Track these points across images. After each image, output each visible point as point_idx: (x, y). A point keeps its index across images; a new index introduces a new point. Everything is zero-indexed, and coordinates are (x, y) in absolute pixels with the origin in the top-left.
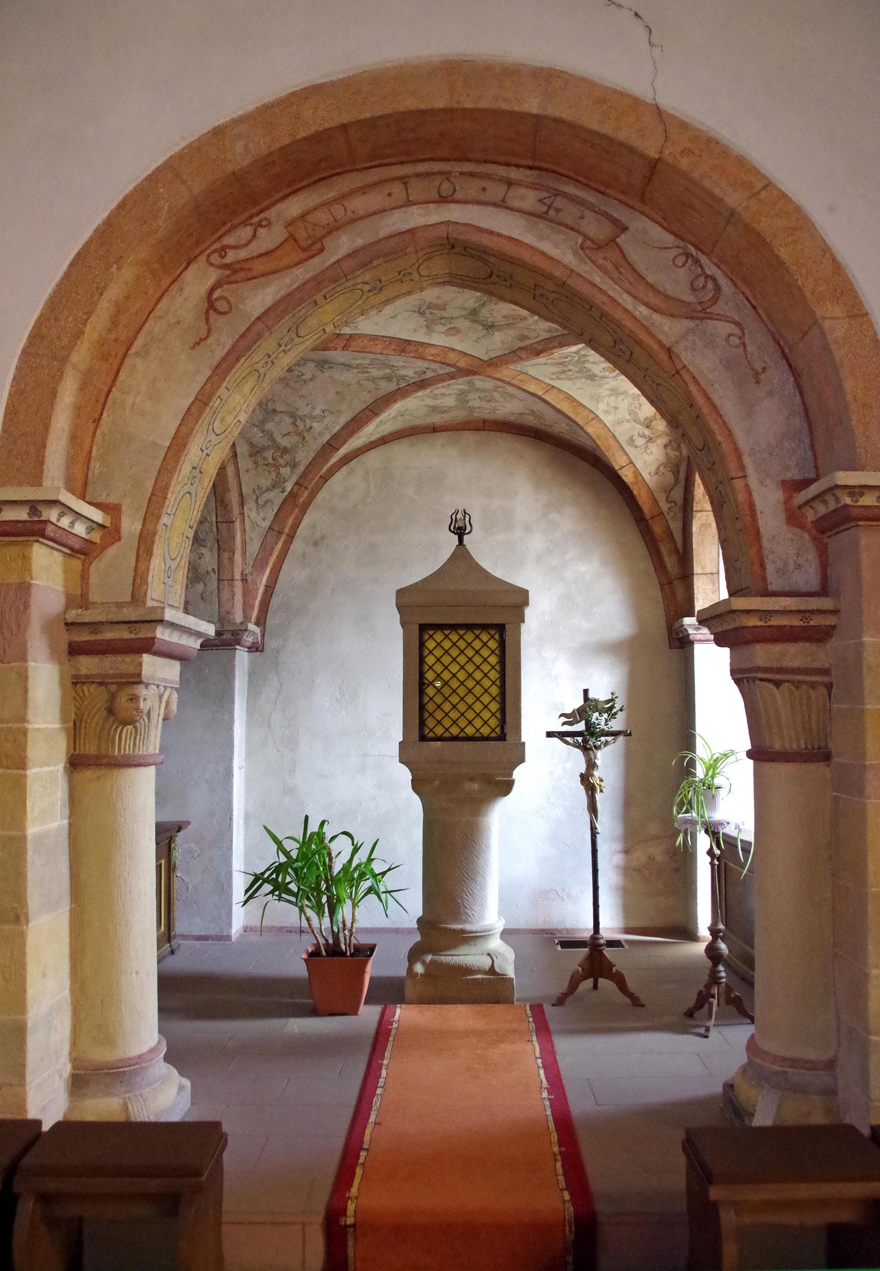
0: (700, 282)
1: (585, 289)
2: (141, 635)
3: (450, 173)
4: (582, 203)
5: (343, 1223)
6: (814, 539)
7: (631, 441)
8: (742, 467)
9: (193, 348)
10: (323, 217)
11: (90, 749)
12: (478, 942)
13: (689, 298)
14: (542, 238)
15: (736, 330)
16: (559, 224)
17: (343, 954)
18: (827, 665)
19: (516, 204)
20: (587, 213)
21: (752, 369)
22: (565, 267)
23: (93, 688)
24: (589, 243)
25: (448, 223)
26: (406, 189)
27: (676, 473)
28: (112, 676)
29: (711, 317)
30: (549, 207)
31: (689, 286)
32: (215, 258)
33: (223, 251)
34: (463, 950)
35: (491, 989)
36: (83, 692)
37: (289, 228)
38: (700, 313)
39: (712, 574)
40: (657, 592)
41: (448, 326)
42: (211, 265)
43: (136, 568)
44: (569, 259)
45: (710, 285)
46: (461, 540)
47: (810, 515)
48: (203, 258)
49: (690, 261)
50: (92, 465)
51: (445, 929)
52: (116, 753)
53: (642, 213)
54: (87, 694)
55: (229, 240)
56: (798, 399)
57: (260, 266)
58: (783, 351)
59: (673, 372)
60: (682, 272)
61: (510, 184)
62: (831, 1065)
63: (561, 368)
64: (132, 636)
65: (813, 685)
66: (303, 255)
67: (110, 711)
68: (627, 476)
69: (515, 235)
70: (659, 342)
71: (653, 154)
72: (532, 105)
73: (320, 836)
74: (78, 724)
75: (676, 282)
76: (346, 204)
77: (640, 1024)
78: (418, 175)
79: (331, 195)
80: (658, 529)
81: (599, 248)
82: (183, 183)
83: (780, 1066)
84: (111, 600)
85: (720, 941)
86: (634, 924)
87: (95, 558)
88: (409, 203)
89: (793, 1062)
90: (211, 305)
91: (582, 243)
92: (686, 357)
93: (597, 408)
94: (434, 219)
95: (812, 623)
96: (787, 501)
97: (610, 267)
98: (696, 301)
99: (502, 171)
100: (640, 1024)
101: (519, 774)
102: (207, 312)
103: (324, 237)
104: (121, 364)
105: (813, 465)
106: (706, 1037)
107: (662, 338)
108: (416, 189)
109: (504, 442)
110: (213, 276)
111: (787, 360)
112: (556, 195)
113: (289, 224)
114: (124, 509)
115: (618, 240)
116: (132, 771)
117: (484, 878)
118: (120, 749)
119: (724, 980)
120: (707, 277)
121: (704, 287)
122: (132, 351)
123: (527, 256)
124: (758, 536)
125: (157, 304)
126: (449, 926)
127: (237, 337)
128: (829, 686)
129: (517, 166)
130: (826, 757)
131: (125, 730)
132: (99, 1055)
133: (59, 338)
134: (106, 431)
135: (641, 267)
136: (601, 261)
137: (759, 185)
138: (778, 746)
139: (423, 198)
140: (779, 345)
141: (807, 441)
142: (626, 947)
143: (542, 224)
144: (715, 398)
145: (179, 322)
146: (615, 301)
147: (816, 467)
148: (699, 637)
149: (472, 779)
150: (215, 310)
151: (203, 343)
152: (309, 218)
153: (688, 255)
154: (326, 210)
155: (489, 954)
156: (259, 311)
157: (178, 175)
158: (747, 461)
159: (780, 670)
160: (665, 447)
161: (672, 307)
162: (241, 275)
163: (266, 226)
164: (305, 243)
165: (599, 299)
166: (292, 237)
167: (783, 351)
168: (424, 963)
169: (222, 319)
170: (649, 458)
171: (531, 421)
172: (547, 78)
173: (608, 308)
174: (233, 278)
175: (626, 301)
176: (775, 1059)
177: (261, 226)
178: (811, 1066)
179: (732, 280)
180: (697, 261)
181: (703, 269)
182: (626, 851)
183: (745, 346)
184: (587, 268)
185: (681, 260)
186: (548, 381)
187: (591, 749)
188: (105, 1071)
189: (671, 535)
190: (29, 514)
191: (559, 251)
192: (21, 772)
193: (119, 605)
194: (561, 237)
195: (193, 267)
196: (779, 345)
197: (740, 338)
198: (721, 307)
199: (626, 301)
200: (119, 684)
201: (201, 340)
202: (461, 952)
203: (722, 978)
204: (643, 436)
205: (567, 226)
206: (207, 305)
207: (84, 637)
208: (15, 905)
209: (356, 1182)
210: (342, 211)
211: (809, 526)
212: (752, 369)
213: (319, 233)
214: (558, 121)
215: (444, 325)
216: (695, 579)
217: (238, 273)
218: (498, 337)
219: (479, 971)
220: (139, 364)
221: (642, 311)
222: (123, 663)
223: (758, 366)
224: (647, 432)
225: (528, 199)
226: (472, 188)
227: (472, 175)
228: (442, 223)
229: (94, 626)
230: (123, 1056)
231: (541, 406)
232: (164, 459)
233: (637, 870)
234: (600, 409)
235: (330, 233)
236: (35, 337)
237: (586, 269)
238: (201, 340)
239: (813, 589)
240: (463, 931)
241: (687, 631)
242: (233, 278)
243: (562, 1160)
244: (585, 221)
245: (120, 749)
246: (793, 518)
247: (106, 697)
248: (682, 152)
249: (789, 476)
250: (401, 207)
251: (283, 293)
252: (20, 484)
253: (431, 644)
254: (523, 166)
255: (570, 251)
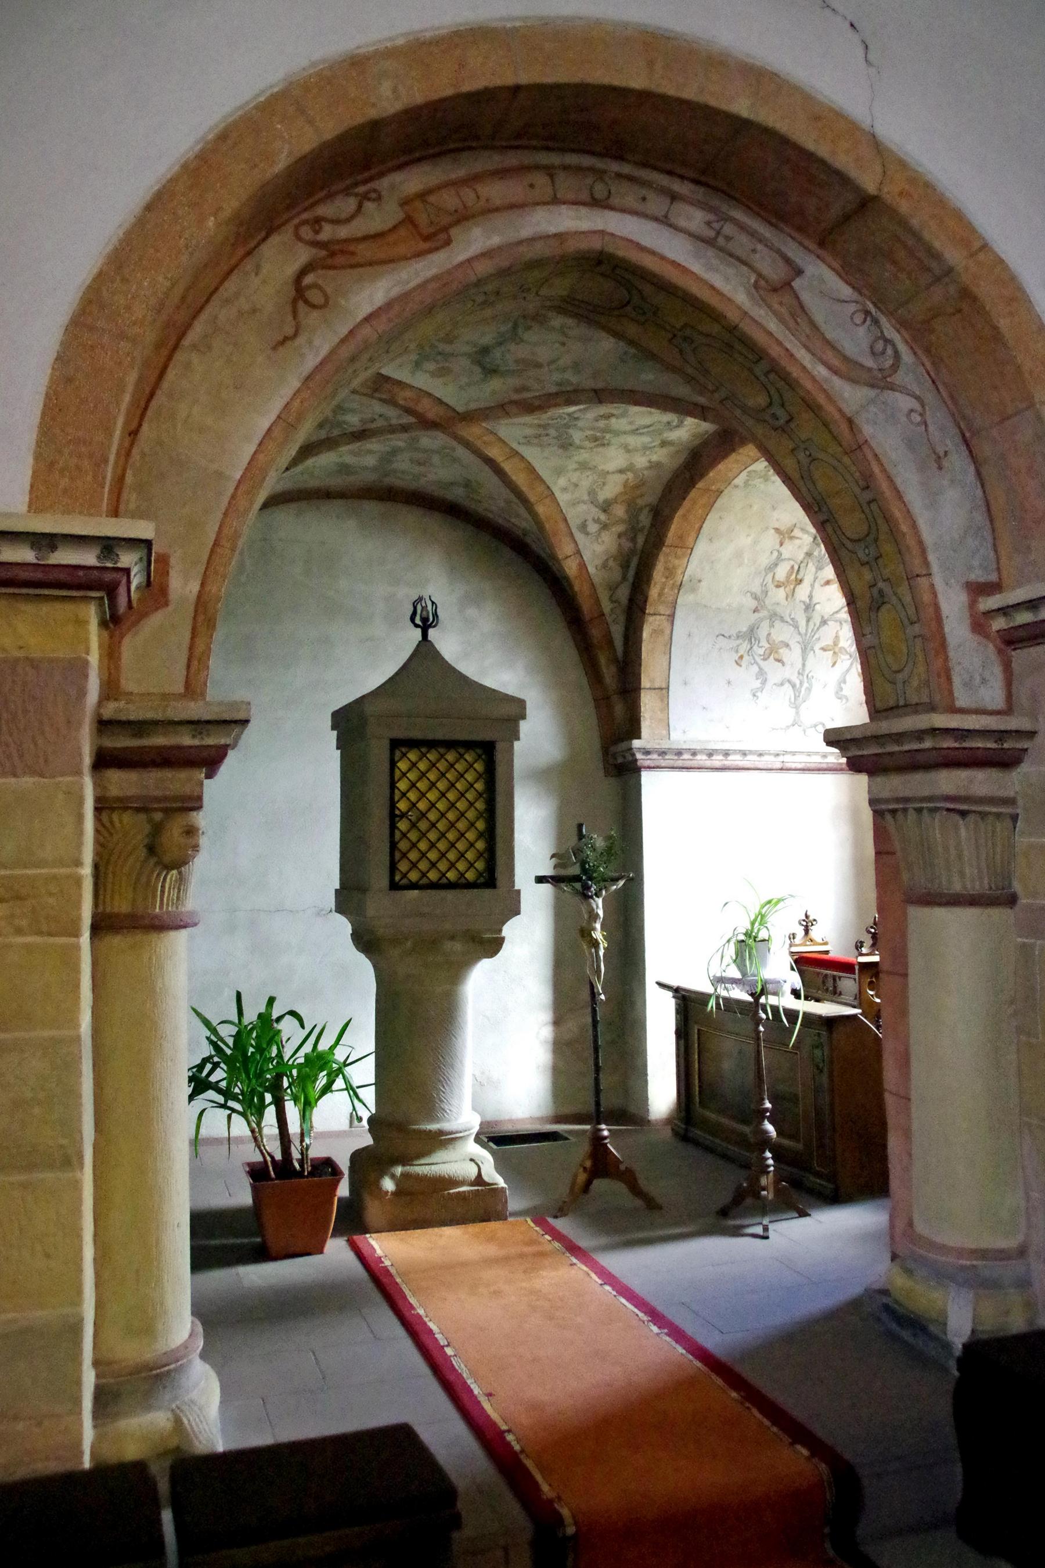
0: (879, 346)
1: (760, 338)
2: (210, 741)
3: (605, 172)
4: (753, 234)
5: (561, 1535)
6: (1000, 652)
7: (583, 527)
8: (926, 564)
9: (274, 348)
10: (449, 200)
11: (121, 905)
12: (458, 1144)
13: (869, 362)
14: (710, 268)
15: (916, 405)
16: (731, 255)
17: (300, 1174)
18: (1012, 794)
19: (682, 223)
20: (760, 247)
21: (935, 453)
22: (739, 308)
23: (127, 818)
24: (762, 283)
25: (602, 233)
26: (553, 182)
27: (625, 566)
28: (157, 799)
29: (892, 388)
30: (718, 233)
31: (868, 350)
32: (306, 232)
33: (317, 223)
34: (440, 1156)
35: (478, 1206)
36: (112, 822)
37: (406, 207)
38: (881, 381)
39: (662, 689)
40: (590, 710)
41: (441, 365)
42: (299, 238)
43: (191, 648)
44: (741, 298)
45: (889, 351)
46: (425, 635)
47: (999, 624)
48: (289, 228)
49: (868, 322)
50: (125, 496)
51: (414, 1130)
52: (157, 910)
53: (818, 257)
54: (118, 825)
55: (324, 210)
56: (979, 492)
57: (364, 251)
58: (963, 436)
59: (855, 447)
60: (861, 331)
61: (674, 197)
62: (1022, 1252)
63: (541, 431)
64: (196, 742)
65: (998, 815)
66: (424, 246)
67: (151, 850)
68: (571, 568)
69: (681, 259)
70: (840, 410)
71: (871, 188)
72: (742, 107)
73: (266, 1021)
74: (102, 869)
75: (855, 341)
76: (479, 188)
77: (677, 1231)
78: (566, 168)
79: (461, 173)
80: (595, 633)
81: (775, 290)
82: (311, 122)
83: (967, 1260)
84: (155, 691)
85: (766, 1122)
86: (567, 1110)
87: (129, 630)
88: (555, 201)
89: (983, 1254)
90: (300, 292)
91: (756, 282)
92: (868, 430)
93: (555, 483)
94: (585, 225)
95: (1006, 746)
96: (972, 604)
97: (787, 316)
98: (875, 367)
99: (663, 180)
100: (677, 1231)
101: (509, 930)
102: (294, 302)
103: (451, 225)
104: (170, 358)
105: (995, 566)
106: (767, 1238)
107: (843, 406)
108: (566, 184)
109: (411, 516)
110: (304, 255)
111: (968, 445)
112: (726, 220)
113: (405, 203)
114: (173, 561)
115: (793, 284)
116: (173, 934)
117: (461, 1062)
118: (161, 907)
119: (772, 1169)
120: (887, 341)
121: (883, 352)
122: (186, 342)
123: (695, 289)
124: (943, 645)
125: (222, 282)
126: (423, 1127)
127: (337, 340)
128: (1015, 818)
129: (682, 177)
130: (1012, 900)
131: (169, 877)
132: (130, 1352)
133: (128, 308)
134: (147, 450)
135: (819, 318)
136: (776, 306)
137: (977, 245)
138: (957, 887)
139: (571, 196)
140: (960, 428)
141: (990, 538)
142: (573, 1139)
143: (711, 252)
144: (898, 481)
145: (254, 311)
146: (792, 355)
147: (998, 569)
148: (647, 763)
149: (452, 938)
150: (306, 302)
151: (289, 343)
152: (432, 199)
153: (867, 313)
154: (453, 192)
155: (472, 1160)
156: (366, 310)
157: (301, 110)
158: (931, 557)
159: (966, 799)
160: (620, 536)
161: (849, 369)
162: (340, 260)
163: (374, 200)
164: (426, 231)
165: (775, 351)
166: (409, 220)
167: (963, 436)
168: (393, 1177)
169: (315, 314)
170: (599, 549)
171: (456, 494)
172: (759, 78)
173: (784, 362)
174: (329, 261)
175: (803, 356)
176: (960, 1252)
177: (369, 199)
178: (1001, 1255)
179: (912, 348)
180: (876, 322)
181: (882, 332)
182: (557, 1022)
183: (926, 426)
184: (762, 312)
185: (859, 318)
186: (514, 445)
187: (591, 897)
188: (143, 1375)
189: (610, 642)
190: (98, 557)
191: (729, 287)
192: (73, 940)
193: (165, 697)
194: (731, 271)
195: (275, 239)
196: (960, 428)
197: (921, 415)
198: (901, 377)
199: (803, 356)
200: (167, 811)
201: (286, 339)
202: (435, 1161)
203: (769, 1166)
204: (597, 521)
205: (739, 259)
206: (293, 293)
207: (123, 742)
208: (64, 1142)
209: (539, 1478)
210: (472, 195)
211: (994, 634)
212: (935, 453)
213: (445, 220)
214: (766, 131)
215: (437, 362)
216: (642, 695)
217: (335, 256)
218: (496, 384)
219: (462, 1183)
220: (195, 358)
221: (821, 371)
222: (173, 781)
223: (941, 451)
224: (603, 517)
225: (695, 218)
226: (629, 196)
227: (630, 179)
228: (595, 232)
229: (140, 727)
230: (165, 1349)
231: (486, 475)
232: (233, 497)
233: (569, 1044)
234: (559, 484)
235: (458, 222)
236: (90, 302)
237: (760, 313)
238: (286, 339)
239: (999, 707)
240: (441, 1133)
241: (634, 755)
242: (329, 261)
243: (754, 1405)
244: (758, 256)
245: (161, 907)
246: (979, 624)
247: (147, 828)
248: (901, 194)
249: (972, 577)
250: (545, 203)
251: (395, 292)
252: (67, 511)
253: (403, 765)
254: (687, 179)
255: (742, 289)
